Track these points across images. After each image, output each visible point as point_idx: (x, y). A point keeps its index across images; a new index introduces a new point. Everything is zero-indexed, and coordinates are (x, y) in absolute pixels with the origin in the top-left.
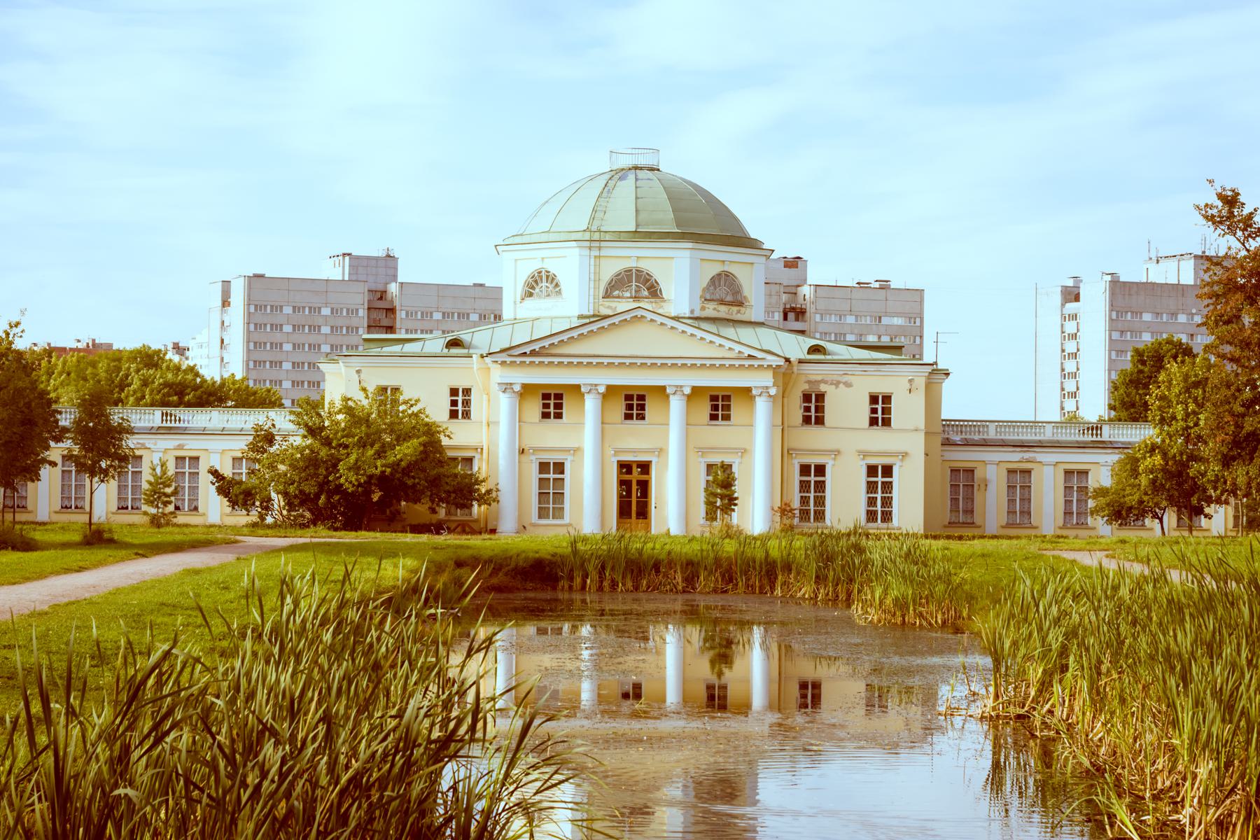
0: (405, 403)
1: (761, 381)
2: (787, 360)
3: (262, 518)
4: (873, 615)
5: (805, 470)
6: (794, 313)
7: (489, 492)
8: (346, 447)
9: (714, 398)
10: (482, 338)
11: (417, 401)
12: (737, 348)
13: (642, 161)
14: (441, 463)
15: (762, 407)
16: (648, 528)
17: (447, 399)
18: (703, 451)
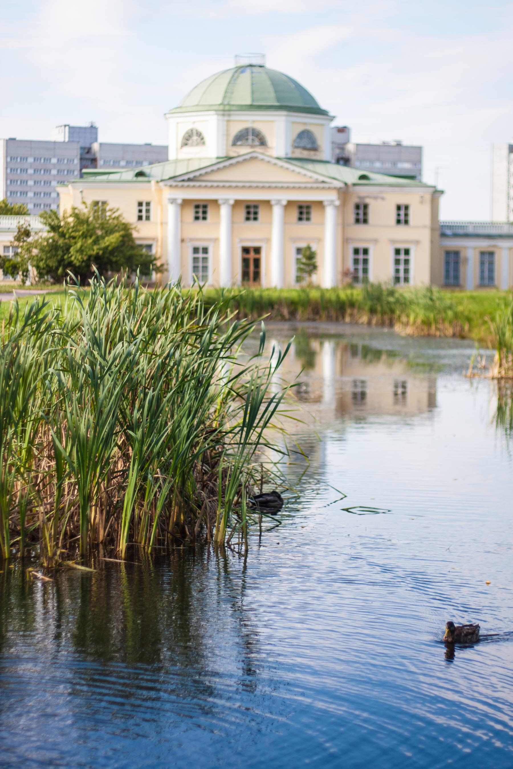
0: (111, 210)
1: (330, 197)
2: (346, 184)
3: (24, 282)
4: (409, 330)
5: (356, 251)
6: (344, 160)
7: (162, 265)
8: (74, 238)
9: (300, 207)
10: (156, 171)
11: (118, 210)
12: (315, 176)
13: (254, 62)
14: (133, 247)
15: (330, 213)
16: (260, 284)
17: (136, 208)
18: (294, 240)
